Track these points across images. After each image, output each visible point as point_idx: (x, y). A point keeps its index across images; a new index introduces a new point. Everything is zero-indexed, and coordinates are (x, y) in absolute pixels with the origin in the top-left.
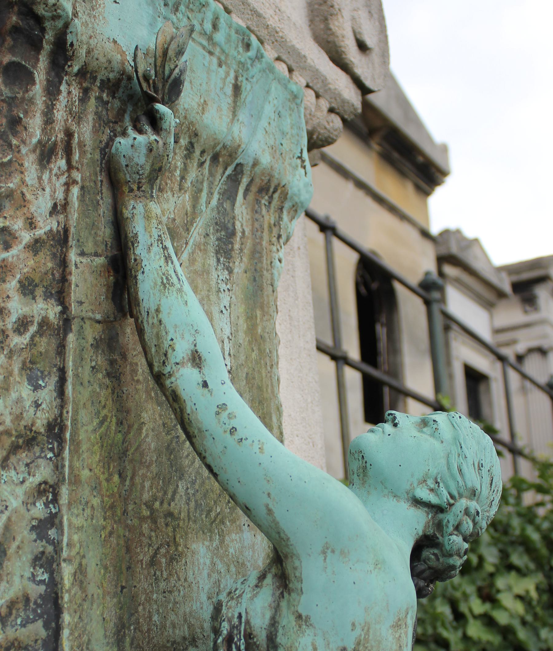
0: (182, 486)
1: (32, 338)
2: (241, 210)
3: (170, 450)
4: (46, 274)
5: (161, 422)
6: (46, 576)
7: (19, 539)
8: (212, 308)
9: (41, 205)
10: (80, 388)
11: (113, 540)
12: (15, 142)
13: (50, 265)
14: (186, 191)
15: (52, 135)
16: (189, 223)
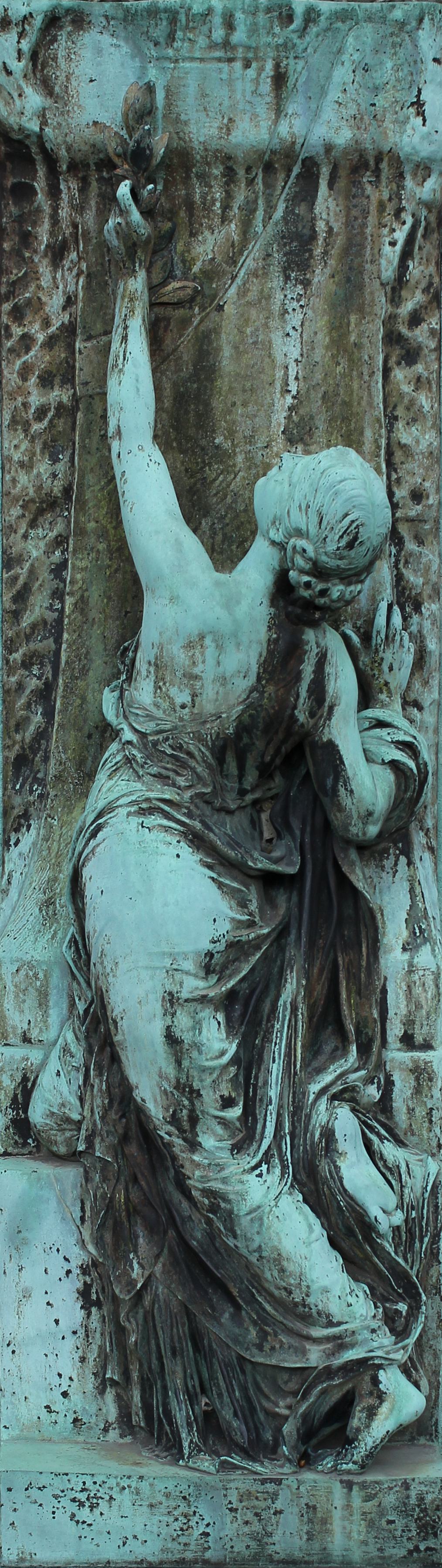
1: (51, 421)
4: (61, 363)
5: (183, 468)
7: (41, 579)
8: (272, 335)
9: (56, 302)
10: (88, 457)
11: (119, 576)
13: (63, 355)
14: (231, 221)
15: (59, 234)
16: (236, 255)
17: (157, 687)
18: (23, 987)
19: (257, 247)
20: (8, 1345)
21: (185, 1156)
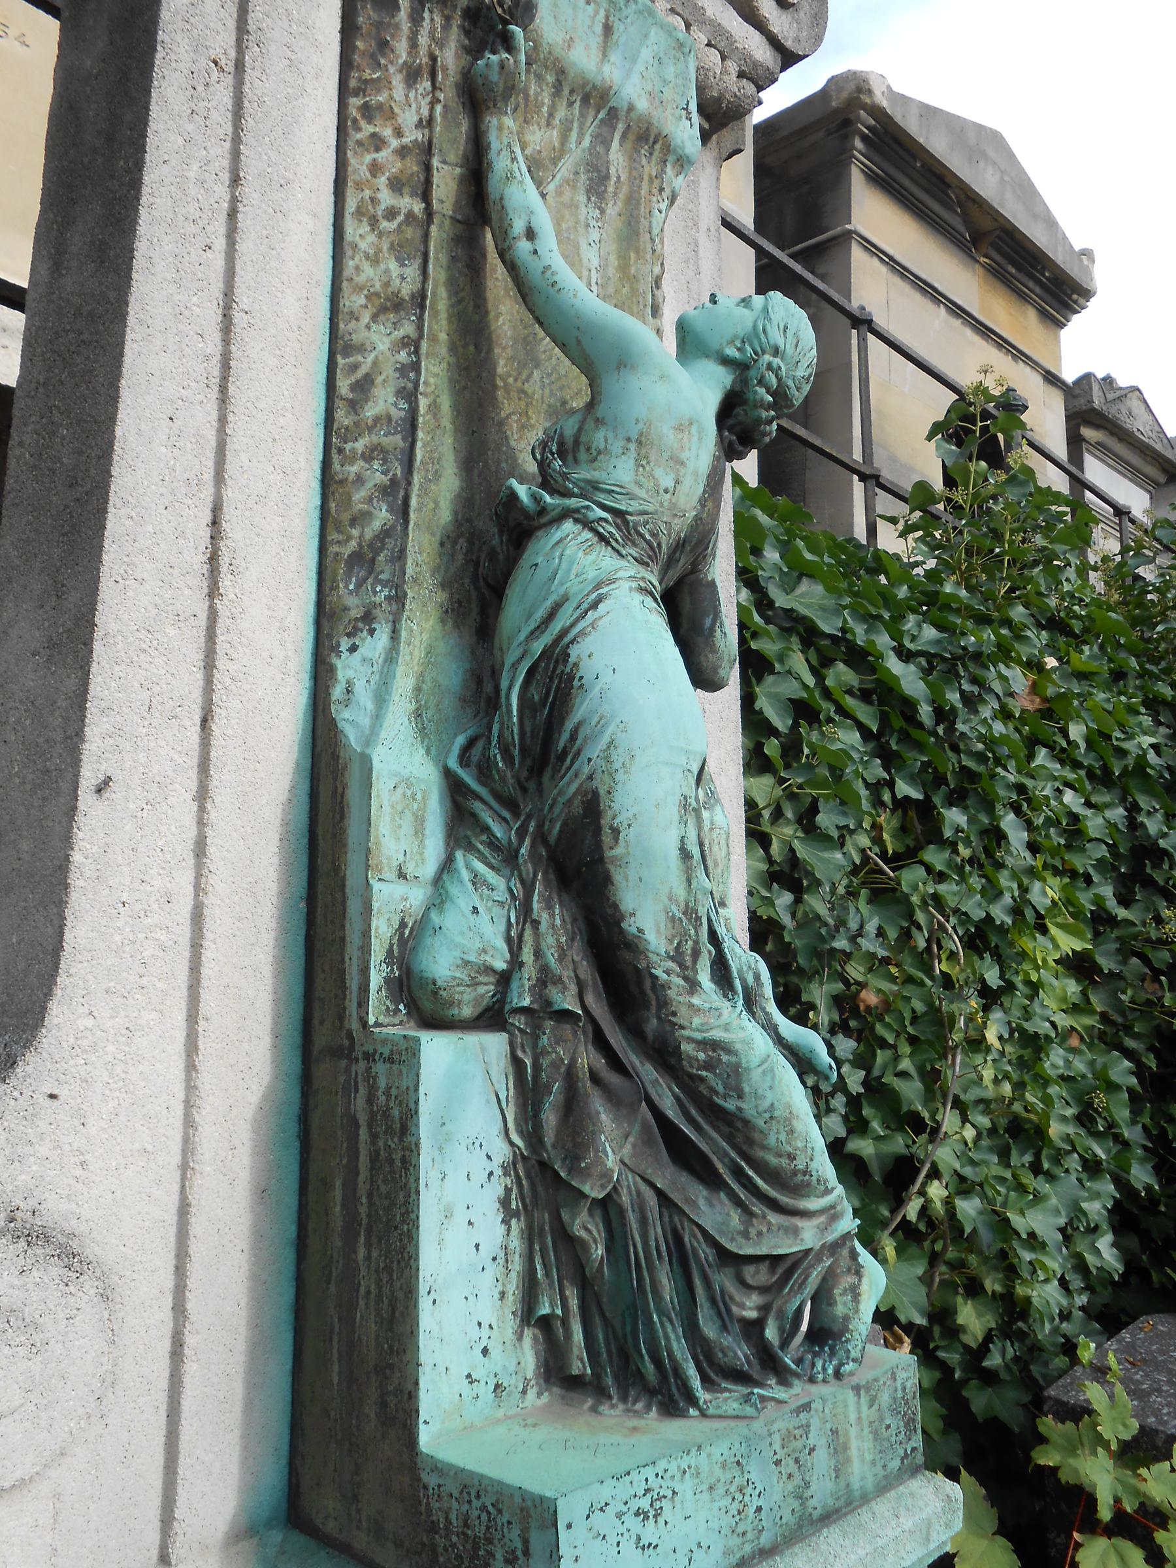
0: (536, 374)
1: (400, 225)
2: (617, 157)
3: (526, 341)
4: (412, 175)
6: (406, 406)
9: (408, 118)
12: (383, 61)
17: (638, 465)
18: (399, 808)
19: (570, 161)
20: (429, 1293)
21: (681, 999)
